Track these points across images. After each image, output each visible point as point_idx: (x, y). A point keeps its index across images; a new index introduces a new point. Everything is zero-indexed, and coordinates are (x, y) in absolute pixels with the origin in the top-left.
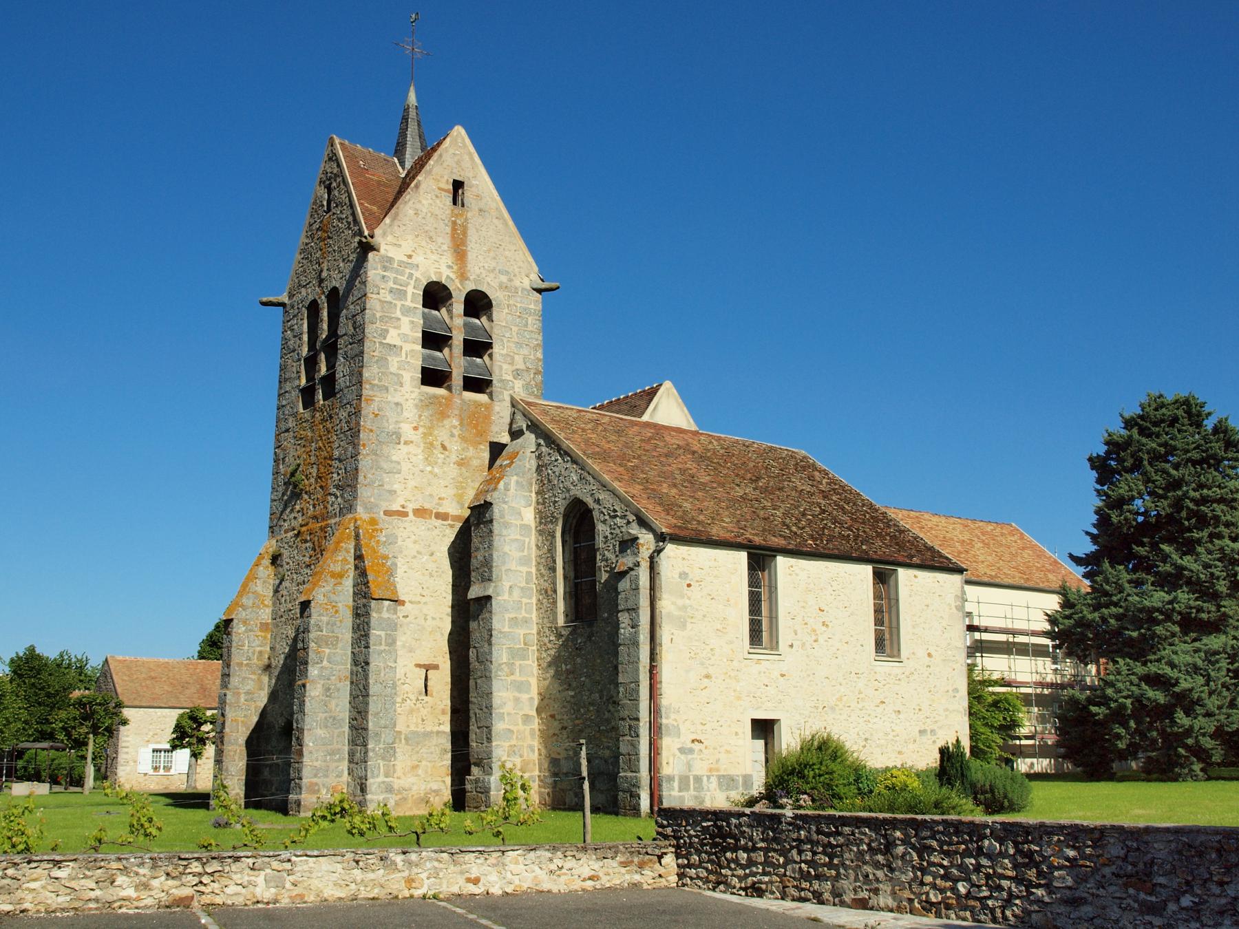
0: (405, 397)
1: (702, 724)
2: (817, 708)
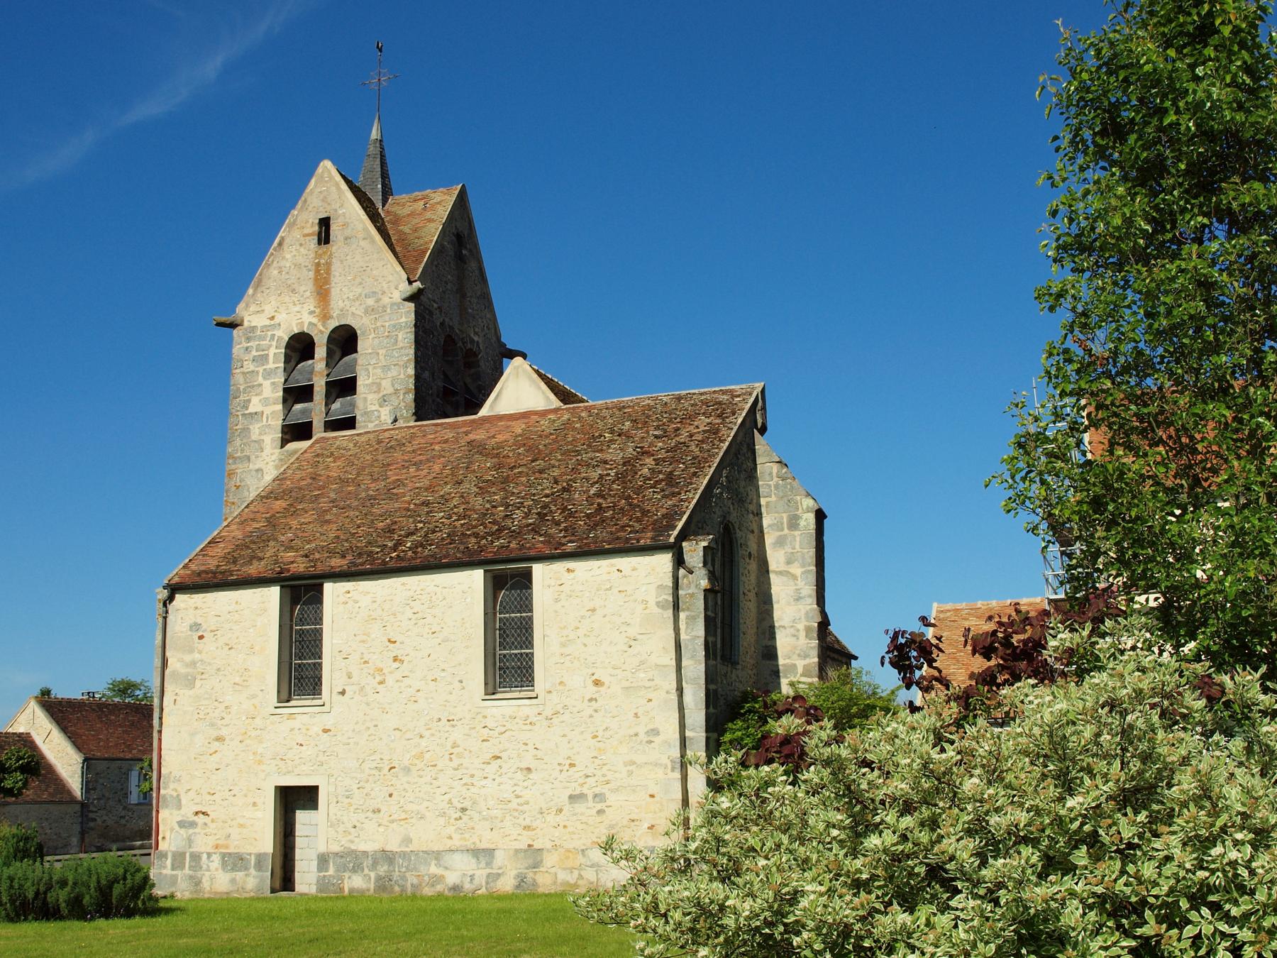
2: (380, 769)
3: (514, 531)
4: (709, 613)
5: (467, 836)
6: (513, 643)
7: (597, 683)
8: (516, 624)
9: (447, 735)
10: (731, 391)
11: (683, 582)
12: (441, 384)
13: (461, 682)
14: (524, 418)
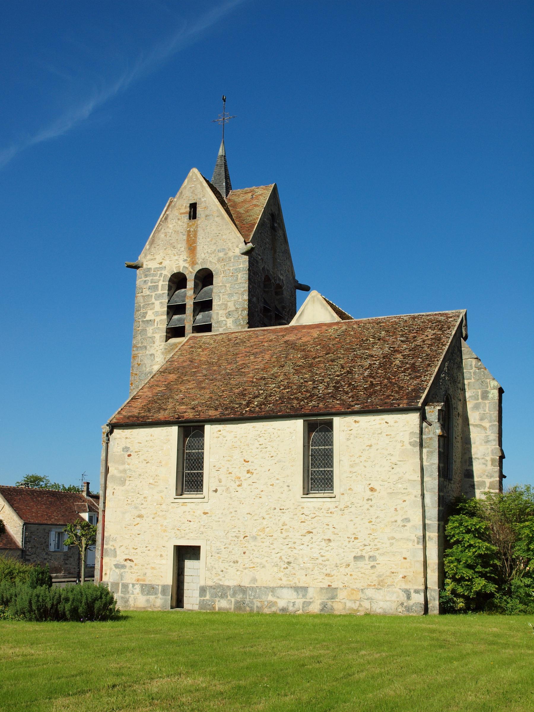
2: (238, 537)
3: (320, 397)
4: (441, 450)
5: (291, 578)
6: (320, 464)
7: (372, 490)
8: (321, 452)
9: (279, 518)
10: (446, 314)
11: (425, 430)
12: (262, 305)
13: (288, 486)
14: (317, 327)
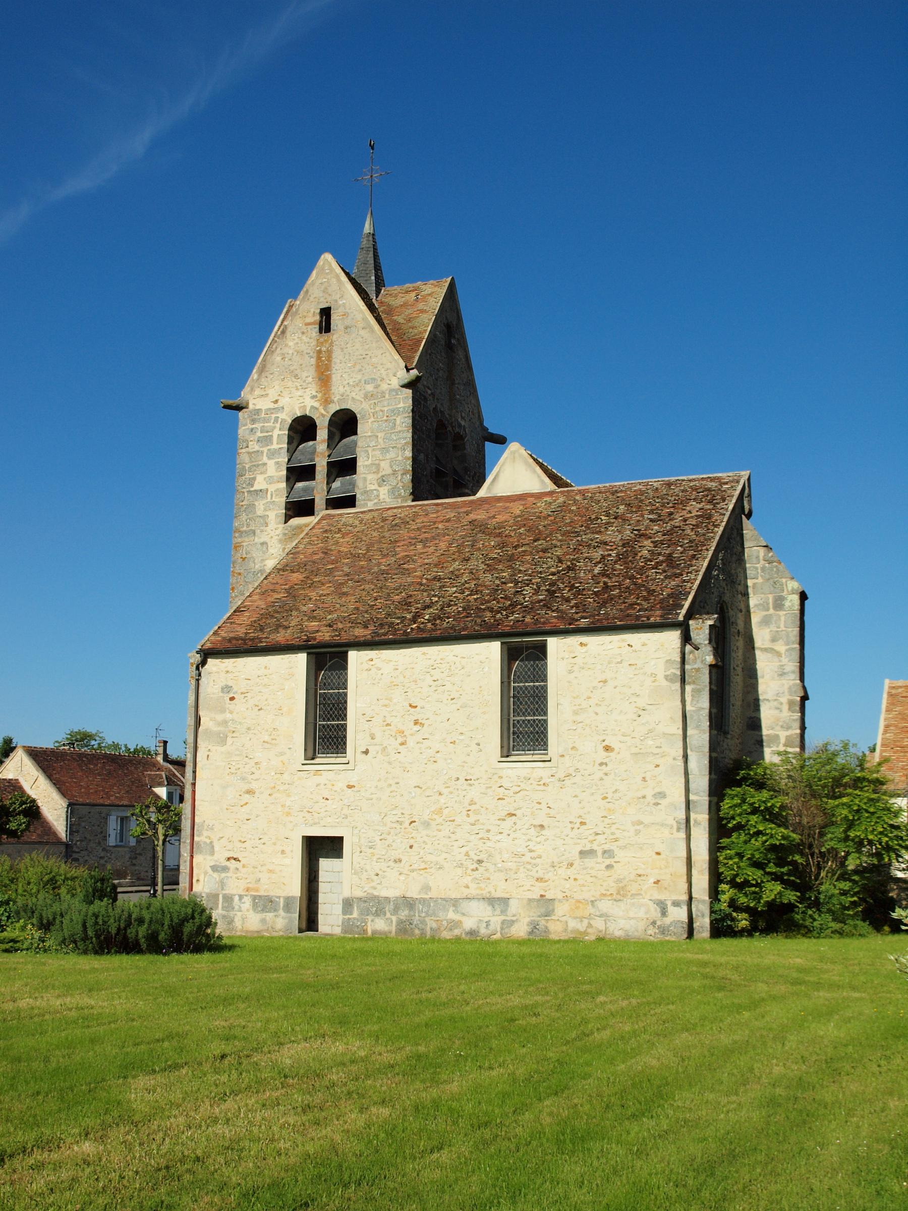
0: (270, 536)
1: (240, 841)
2: (401, 823)
3: (527, 606)
4: (714, 687)
5: (482, 885)
6: (526, 710)
7: (607, 749)
8: (529, 692)
9: (464, 793)
10: (718, 478)
12: (433, 466)
13: (478, 744)
